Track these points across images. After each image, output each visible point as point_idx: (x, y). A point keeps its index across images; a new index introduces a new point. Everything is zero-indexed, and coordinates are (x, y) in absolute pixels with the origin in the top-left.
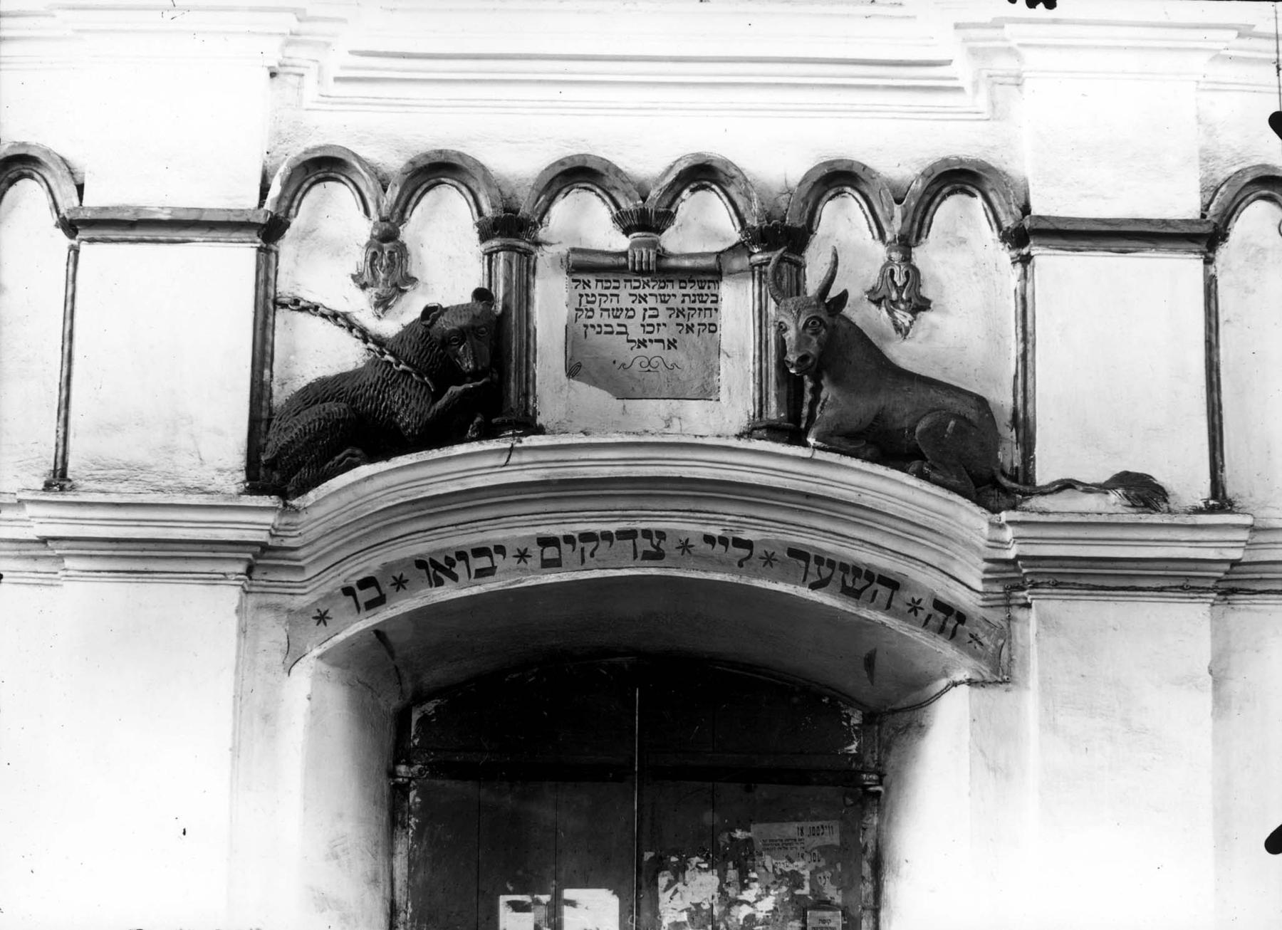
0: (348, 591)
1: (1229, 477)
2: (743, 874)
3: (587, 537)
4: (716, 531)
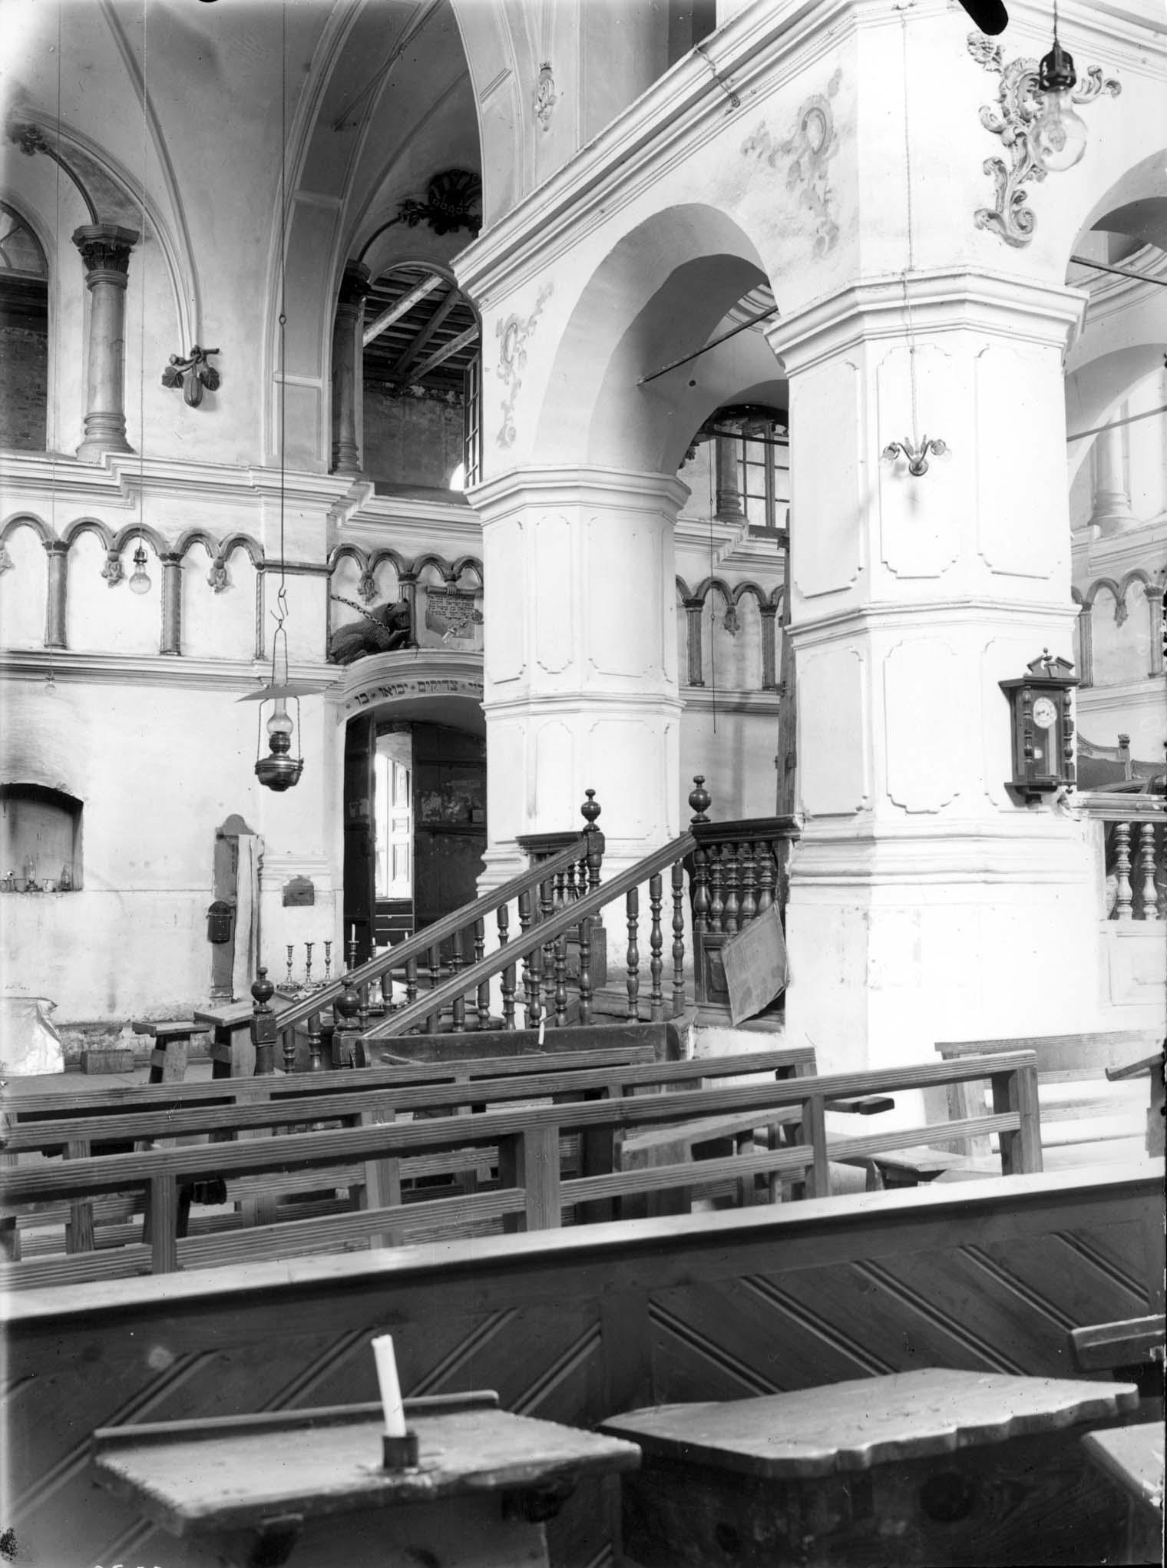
0: (357, 698)
1: (802, 673)
2: (450, 798)
3: (433, 682)
4: (473, 682)
